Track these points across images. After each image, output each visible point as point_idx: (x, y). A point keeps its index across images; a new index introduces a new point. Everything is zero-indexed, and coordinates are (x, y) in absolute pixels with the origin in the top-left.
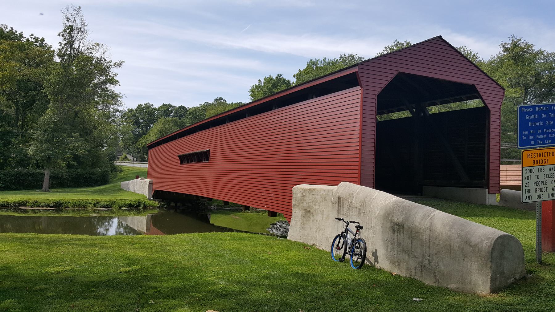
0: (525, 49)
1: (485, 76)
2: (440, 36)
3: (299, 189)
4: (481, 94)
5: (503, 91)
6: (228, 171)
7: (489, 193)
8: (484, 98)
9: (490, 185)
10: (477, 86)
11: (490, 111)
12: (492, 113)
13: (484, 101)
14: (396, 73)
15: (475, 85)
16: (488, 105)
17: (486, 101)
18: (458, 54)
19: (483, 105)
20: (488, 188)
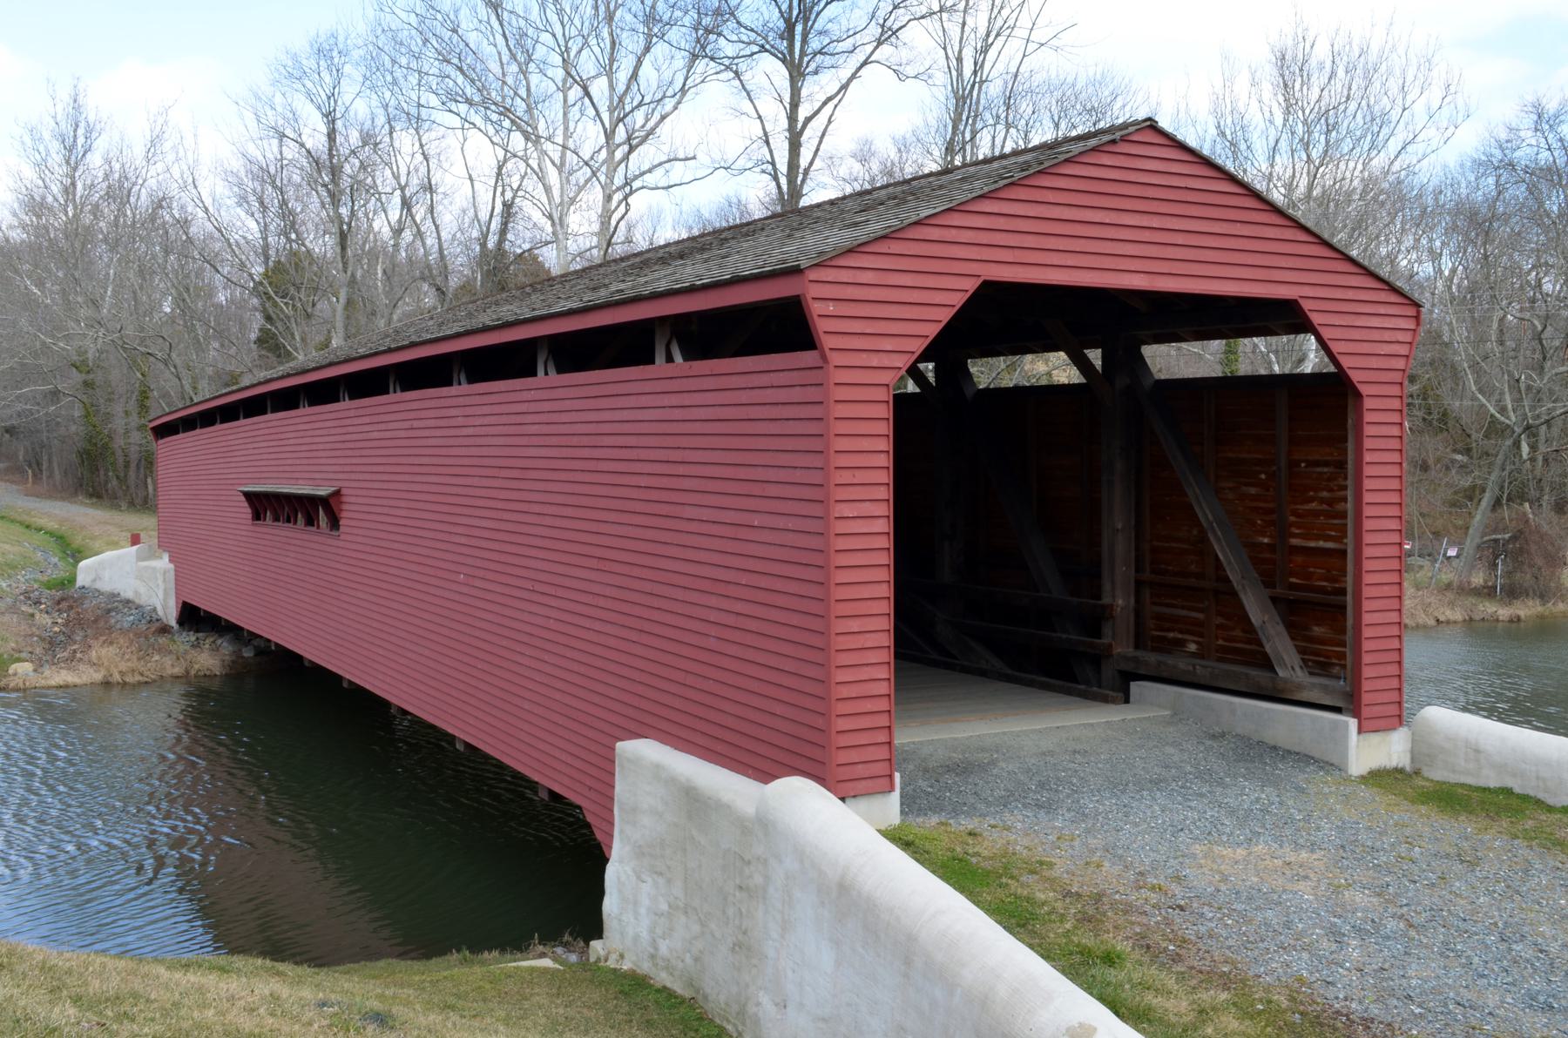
0: (512, 268)
1: (1388, 292)
2: (1149, 119)
3: (621, 746)
4: (1316, 319)
5: (1411, 311)
6: (1155, 222)
7: (1360, 731)
8: (1326, 334)
9: (1366, 698)
10: (1306, 305)
11: (1359, 395)
12: (1368, 403)
13: (1326, 344)
14: (971, 285)
15: (1300, 301)
16: (1346, 362)
17: (1336, 348)
18: (1250, 203)
19: (1332, 369)
20: (1356, 714)
